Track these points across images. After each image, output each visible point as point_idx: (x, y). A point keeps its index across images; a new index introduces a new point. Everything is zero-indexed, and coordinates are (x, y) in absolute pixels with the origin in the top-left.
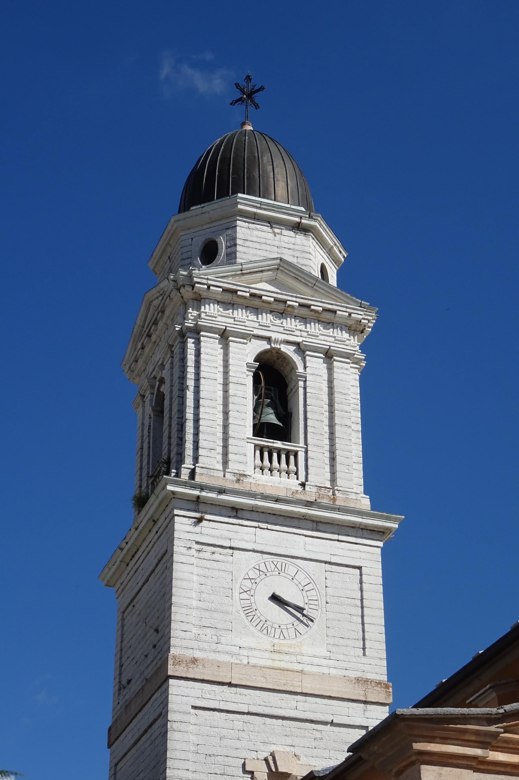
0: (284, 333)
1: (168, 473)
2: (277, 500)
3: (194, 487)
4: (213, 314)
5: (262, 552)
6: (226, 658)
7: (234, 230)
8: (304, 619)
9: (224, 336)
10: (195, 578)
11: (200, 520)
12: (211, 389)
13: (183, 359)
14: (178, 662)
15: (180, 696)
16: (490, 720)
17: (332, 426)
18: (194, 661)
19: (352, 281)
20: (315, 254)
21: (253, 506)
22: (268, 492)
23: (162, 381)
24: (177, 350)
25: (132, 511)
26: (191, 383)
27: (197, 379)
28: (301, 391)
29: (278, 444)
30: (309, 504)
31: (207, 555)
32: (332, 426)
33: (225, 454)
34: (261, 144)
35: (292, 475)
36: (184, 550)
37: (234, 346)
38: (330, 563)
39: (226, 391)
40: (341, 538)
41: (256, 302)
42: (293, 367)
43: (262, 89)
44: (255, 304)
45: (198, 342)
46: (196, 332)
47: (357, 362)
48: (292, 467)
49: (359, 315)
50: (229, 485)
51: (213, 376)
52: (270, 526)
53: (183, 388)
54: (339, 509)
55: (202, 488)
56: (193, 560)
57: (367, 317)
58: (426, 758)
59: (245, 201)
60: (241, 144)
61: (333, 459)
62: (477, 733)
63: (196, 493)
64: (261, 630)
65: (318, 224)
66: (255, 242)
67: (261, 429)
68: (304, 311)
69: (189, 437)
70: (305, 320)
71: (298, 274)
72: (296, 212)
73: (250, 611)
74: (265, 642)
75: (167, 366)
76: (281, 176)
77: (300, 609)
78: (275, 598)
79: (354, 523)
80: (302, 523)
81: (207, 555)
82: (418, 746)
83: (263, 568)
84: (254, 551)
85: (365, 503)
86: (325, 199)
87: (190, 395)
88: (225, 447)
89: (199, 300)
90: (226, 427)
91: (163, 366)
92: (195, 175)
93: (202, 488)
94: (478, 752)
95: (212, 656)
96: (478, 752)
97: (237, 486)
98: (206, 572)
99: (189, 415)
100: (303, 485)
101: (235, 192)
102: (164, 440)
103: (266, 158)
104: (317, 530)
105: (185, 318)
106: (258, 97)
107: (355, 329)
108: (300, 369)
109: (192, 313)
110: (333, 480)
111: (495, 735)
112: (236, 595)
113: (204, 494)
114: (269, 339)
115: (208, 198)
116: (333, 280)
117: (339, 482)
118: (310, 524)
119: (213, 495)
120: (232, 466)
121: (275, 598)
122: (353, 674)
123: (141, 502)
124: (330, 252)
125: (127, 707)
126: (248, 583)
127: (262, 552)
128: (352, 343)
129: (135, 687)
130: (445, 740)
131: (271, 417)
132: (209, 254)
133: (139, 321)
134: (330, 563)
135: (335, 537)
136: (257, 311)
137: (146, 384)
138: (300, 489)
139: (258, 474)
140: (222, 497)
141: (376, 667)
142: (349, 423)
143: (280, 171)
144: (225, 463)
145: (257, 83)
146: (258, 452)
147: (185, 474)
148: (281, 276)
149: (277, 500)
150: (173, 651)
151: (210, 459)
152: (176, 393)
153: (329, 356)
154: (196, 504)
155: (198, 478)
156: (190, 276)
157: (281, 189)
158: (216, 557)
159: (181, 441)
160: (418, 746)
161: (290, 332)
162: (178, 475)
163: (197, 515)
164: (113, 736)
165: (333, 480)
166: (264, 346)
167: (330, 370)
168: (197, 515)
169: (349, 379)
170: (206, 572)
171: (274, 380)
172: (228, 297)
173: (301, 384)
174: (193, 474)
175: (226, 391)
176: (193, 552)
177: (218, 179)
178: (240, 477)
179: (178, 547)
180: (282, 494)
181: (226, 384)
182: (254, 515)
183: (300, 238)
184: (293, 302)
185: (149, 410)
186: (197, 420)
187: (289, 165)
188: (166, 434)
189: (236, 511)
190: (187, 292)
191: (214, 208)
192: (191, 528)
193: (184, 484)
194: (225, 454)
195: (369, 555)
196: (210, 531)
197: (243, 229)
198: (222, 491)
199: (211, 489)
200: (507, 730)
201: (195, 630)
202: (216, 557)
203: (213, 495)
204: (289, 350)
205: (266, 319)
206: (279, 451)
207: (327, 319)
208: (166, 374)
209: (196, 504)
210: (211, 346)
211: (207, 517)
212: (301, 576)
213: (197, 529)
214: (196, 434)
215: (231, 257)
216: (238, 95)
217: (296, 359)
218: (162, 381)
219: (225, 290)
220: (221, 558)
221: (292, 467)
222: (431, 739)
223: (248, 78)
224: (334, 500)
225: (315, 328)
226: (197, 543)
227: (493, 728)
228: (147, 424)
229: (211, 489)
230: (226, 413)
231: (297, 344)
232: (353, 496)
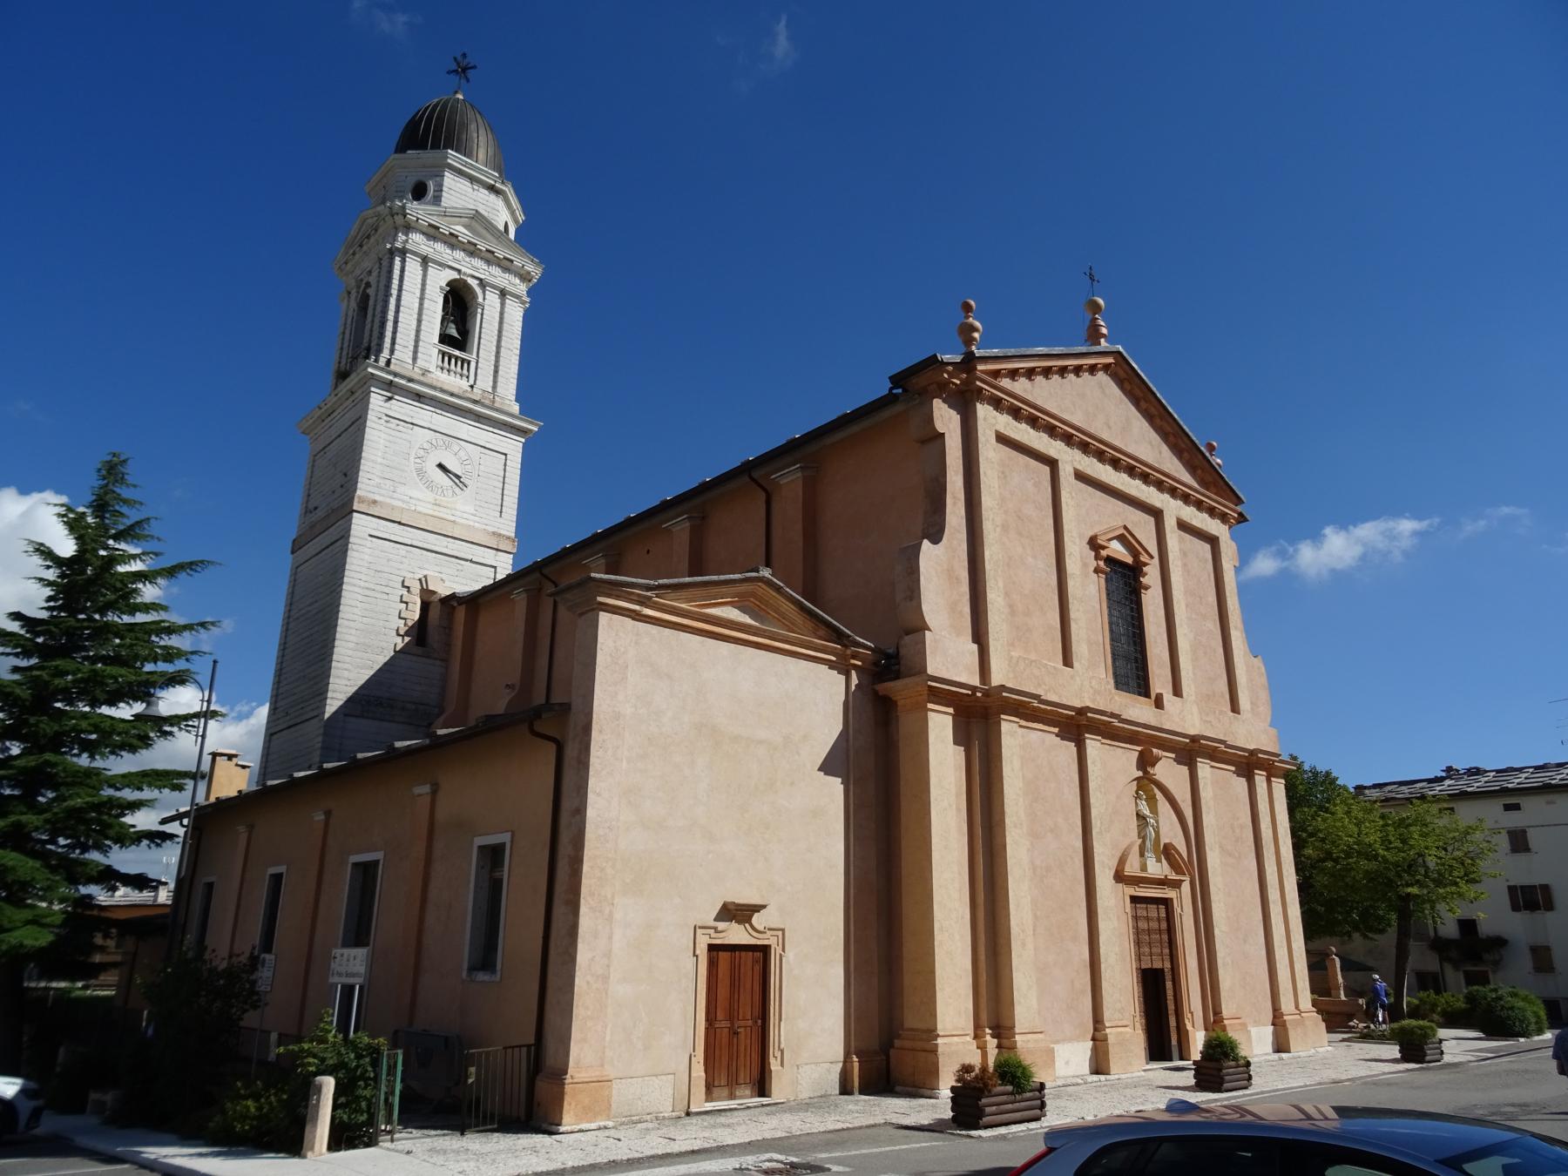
0: (472, 269)
1: (367, 357)
2: (452, 395)
3: (390, 373)
4: (417, 241)
6: (399, 504)
7: (1133, 683)
9: (425, 261)
11: (390, 399)
12: (410, 300)
13: (390, 272)
14: (362, 500)
15: (360, 526)
16: (649, 588)
17: (498, 347)
18: (375, 502)
19: (527, 238)
20: (502, 212)
22: (445, 387)
23: (368, 285)
24: (385, 263)
25: (331, 379)
26: (394, 292)
27: (400, 290)
29: (457, 353)
30: (475, 402)
32: (498, 347)
33: (415, 352)
34: (470, 114)
37: (432, 271)
39: (421, 304)
41: (453, 240)
42: (475, 296)
43: (474, 67)
44: (452, 241)
45: (403, 262)
46: (403, 253)
47: (523, 303)
49: (530, 268)
50: (416, 377)
53: (387, 295)
54: (497, 410)
55: (396, 375)
57: (535, 271)
59: (453, 157)
60: (454, 110)
61: (496, 372)
65: (508, 189)
66: (458, 193)
67: (445, 339)
68: (489, 256)
69: (388, 334)
70: (488, 262)
71: (488, 225)
72: (491, 176)
73: (421, 473)
74: (430, 496)
75: (375, 274)
76: (482, 142)
77: (458, 477)
78: (440, 466)
82: (600, 599)
85: (516, 408)
86: (516, 170)
87: (393, 301)
89: (408, 228)
90: (418, 331)
91: (370, 272)
92: (413, 125)
93: (396, 375)
94: (637, 608)
95: (388, 500)
96: (637, 608)
101: (446, 147)
102: (365, 329)
103: (473, 127)
105: (395, 240)
106: (470, 73)
107: (525, 277)
108: (480, 300)
109: (401, 237)
110: (494, 387)
111: (650, 598)
114: (459, 271)
115: (421, 145)
116: (512, 235)
120: (420, 362)
121: (440, 466)
122: (491, 529)
123: (342, 375)
124: (513, 213)
125: (312, 527)
128: (521, 288)
129: (320, 514)
130: (618, 597)
131: (453, 331)
132: (419, 192)
133: (353, 233)
136: (453, 247)
137: (353, 283)
139: (439, 373)
141: (508, 526)
143: (482, 139)
144: (415, 359)
145: (470, 60)
147: (382, 362)
148: (474, 223)
149: (452, 395)
150: (358, 492)
151: (403, 354)
152: (381, 297)
153: (503, 294)
154: (389, 386)
155: (392, 367)
156: (404, 207)
157: (481, 155)
159: (382, 336)
160: (600, 599)
161: (476, 269)
162: (376, 361)
164: (296, 547)
165: (494, 387)
166: (455, 275)
167: (503, 304)
169: (515, 314)
171: (459, 303)
172: (432, 231)
174: (388, 363)
175: (421, 304)
177: (430, 133)
178: (425, 372)
179: (371, 416)
180: (456, 391)
181: (422, 299)
183: (492, 197)
184: (482, 246)
185: (353, 304)
186: (396, 322)
187: (491, 142)
188: (368, 327)
189: (419, 397)
190: (399, 219)
191: (428, 156)
194: (415, 352)
195: (514, 447)
197: (449, 179)
198: (410, 380)
199: (403, 377)
201: (378, 480)
204: (473, 283)
205: (459, 255)
206: (457, 358)
207: (506, 265)
208: (372, 279)
209: (389, 386)
210: (413, 266)
212: (462, 453)
214: (395, 332)
215: (437, 200)
216: (454, 67)
217: (478, 290)
218: (368, 285)
219: (431, 225)
222: (609, 596)
223: (464, 55)
225: (495, 270)
228: (350, 313)
229: (403, 377)
230: (419, 321)
231: (481, 280)
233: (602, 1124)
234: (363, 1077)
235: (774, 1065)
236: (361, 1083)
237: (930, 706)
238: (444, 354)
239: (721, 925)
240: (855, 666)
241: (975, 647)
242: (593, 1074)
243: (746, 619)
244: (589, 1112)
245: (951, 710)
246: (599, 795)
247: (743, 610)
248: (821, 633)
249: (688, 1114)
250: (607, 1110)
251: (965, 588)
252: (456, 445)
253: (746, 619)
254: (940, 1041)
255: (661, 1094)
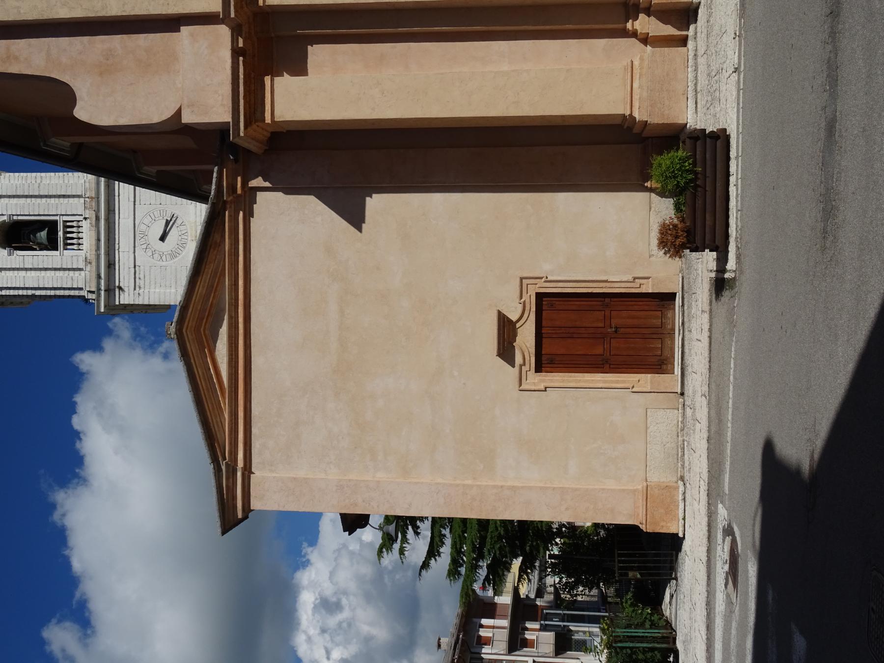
2: (99, 240)
5: (135, 247)
8: (174, 219)
10: (157, 290)
11: (120, 288)
21: (105, 254)
22: (94, 242)
28: (20, 218)
29: (61, 234)
31: (142, 282)
35: (80, 224)
36: (141, 298)
38: (135, 202)
40: (117, 194)
48: (74, 224)
51: (22, 279)
52: (117, 242)
56: (146, 291)
58: (246, 506)
62: (227, 479)
63: (103, 293)
64: (184, 248)
67: (52, 245)
73: (173, 255)
77: (167, 222)
78: (162, 239)
79: (105, 186)
80: (111, 221)
81: (142, 282)
83: (144, 246)
84: (134, 252)
88: (69, 269)
94: (239, 474)
96: (239, 474)
97: (94, 264)
98: (153, 282)
99: (52, 293)
100: (85, 219)
104: (114, 210)
110: (79, 196)
112: (164, 263)
113: (103, 288)
117: (79, 193)
118: (111, 215)
119: (102, 282)
121: (162, 239)
126: (156, 256)
127: (135, 247)
130: (234, 498)
131: (43, 234)
134: (135, 202)
135: (117, 198)
138: (88, 221)
140: (103, 276)
142: (37, 185)
146: (69, 247)
147: (90, 296)
158: (142, 276)
163: (117, 290)
165: (79, 196)
168: (117, 290)
170: (153, 282)
173: (15, 218)
176: (142, 291)
178: (87, 261)
179: (139, 301)
182: (111, 253)
189: (111, 265)
192: (126, 294)
193: (99, 295)
196: (126, 281)
200: (224, 459)
202: (142, 276)
203: (102, 282)
206: (65, 233)
211: (117, 284)
212: (147, 221)
213: (126, 289)
220: (142, 273)
221: (74, 241)
224: (92, 198)
226: (135, 289)
227: (224, 468)
229: (99, 284)
232: (87, 185)
233: (681, 497)
234: (630, 656)
235: (648, 288)
236: (634, 657)
237: (268, 120)
238: (66, 244)
239: (518, 359)
240: (245, 183)
241: (183, 29)
242: (641, 503)
243: (224, 330)
244: (670, 510)
245: (267, 79)
246: (410, 505)
247: (215, 337)
248: (217, 237)
249: (682, 394)
250: (669, 489)
251: (116, 42)
252: (141, 228)
253: (224, 330)
254: (636, 114)
255: (663, 421)
